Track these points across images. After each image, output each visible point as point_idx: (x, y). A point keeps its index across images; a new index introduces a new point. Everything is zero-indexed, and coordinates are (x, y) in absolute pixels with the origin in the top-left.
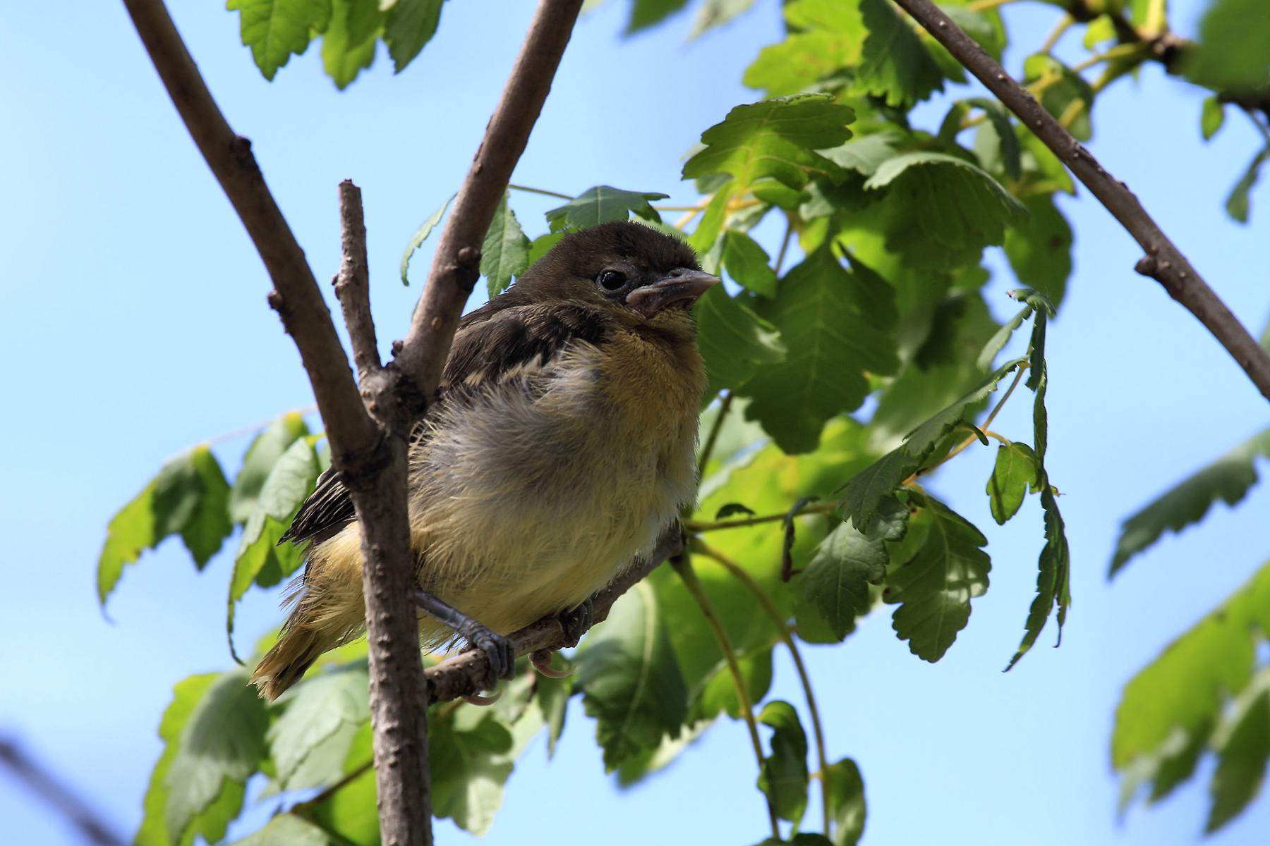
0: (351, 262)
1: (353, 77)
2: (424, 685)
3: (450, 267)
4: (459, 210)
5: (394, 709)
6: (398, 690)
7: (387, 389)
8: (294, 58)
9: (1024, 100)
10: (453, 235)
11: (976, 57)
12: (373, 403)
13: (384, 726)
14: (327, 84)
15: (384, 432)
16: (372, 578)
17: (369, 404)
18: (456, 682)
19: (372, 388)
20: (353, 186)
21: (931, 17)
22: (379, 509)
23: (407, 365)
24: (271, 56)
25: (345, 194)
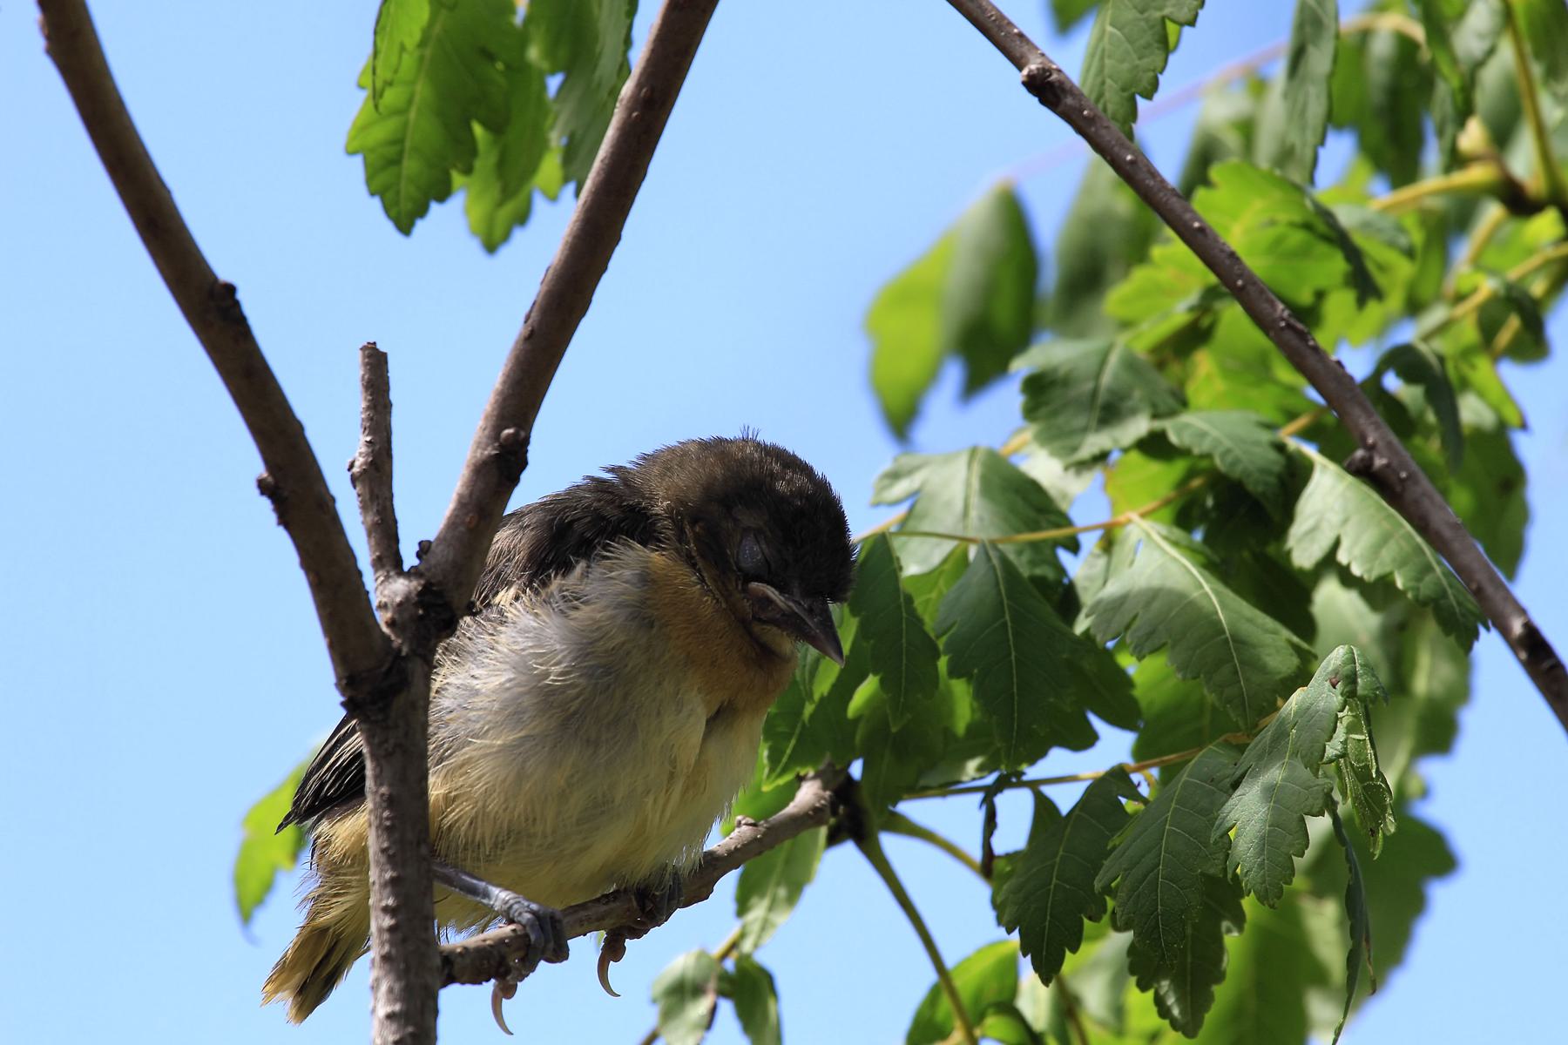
0: (370, 442)
1: (506, 237)
2: (438, 961)
3: (490, 451)
4: (504, 382)
5: (397, 987)
6: (402, 966)
7: (407, 598)
8: (435, 208)
9: (1223, 256)
10: (495, 413)
11: (1168, 200)
12: (389, 615)
13: (383, 1010)
14: (474, 247)
15: (399, 650)
16: (377, 828)
17: (382, 618)
18: (485, 962)
19: (389, 597)
20: (377, 350)
21: (1116, 149)
22: (389, 746)
23: (433, 570)
24: (406, 206)
25: (367, 360)
